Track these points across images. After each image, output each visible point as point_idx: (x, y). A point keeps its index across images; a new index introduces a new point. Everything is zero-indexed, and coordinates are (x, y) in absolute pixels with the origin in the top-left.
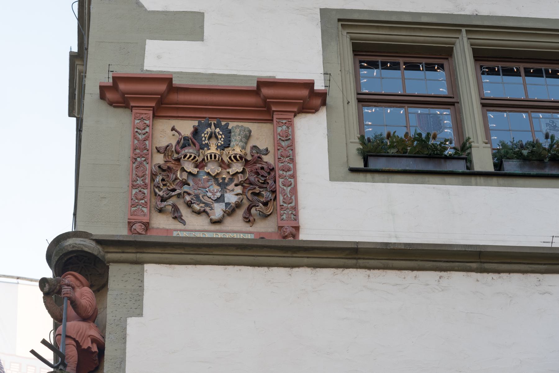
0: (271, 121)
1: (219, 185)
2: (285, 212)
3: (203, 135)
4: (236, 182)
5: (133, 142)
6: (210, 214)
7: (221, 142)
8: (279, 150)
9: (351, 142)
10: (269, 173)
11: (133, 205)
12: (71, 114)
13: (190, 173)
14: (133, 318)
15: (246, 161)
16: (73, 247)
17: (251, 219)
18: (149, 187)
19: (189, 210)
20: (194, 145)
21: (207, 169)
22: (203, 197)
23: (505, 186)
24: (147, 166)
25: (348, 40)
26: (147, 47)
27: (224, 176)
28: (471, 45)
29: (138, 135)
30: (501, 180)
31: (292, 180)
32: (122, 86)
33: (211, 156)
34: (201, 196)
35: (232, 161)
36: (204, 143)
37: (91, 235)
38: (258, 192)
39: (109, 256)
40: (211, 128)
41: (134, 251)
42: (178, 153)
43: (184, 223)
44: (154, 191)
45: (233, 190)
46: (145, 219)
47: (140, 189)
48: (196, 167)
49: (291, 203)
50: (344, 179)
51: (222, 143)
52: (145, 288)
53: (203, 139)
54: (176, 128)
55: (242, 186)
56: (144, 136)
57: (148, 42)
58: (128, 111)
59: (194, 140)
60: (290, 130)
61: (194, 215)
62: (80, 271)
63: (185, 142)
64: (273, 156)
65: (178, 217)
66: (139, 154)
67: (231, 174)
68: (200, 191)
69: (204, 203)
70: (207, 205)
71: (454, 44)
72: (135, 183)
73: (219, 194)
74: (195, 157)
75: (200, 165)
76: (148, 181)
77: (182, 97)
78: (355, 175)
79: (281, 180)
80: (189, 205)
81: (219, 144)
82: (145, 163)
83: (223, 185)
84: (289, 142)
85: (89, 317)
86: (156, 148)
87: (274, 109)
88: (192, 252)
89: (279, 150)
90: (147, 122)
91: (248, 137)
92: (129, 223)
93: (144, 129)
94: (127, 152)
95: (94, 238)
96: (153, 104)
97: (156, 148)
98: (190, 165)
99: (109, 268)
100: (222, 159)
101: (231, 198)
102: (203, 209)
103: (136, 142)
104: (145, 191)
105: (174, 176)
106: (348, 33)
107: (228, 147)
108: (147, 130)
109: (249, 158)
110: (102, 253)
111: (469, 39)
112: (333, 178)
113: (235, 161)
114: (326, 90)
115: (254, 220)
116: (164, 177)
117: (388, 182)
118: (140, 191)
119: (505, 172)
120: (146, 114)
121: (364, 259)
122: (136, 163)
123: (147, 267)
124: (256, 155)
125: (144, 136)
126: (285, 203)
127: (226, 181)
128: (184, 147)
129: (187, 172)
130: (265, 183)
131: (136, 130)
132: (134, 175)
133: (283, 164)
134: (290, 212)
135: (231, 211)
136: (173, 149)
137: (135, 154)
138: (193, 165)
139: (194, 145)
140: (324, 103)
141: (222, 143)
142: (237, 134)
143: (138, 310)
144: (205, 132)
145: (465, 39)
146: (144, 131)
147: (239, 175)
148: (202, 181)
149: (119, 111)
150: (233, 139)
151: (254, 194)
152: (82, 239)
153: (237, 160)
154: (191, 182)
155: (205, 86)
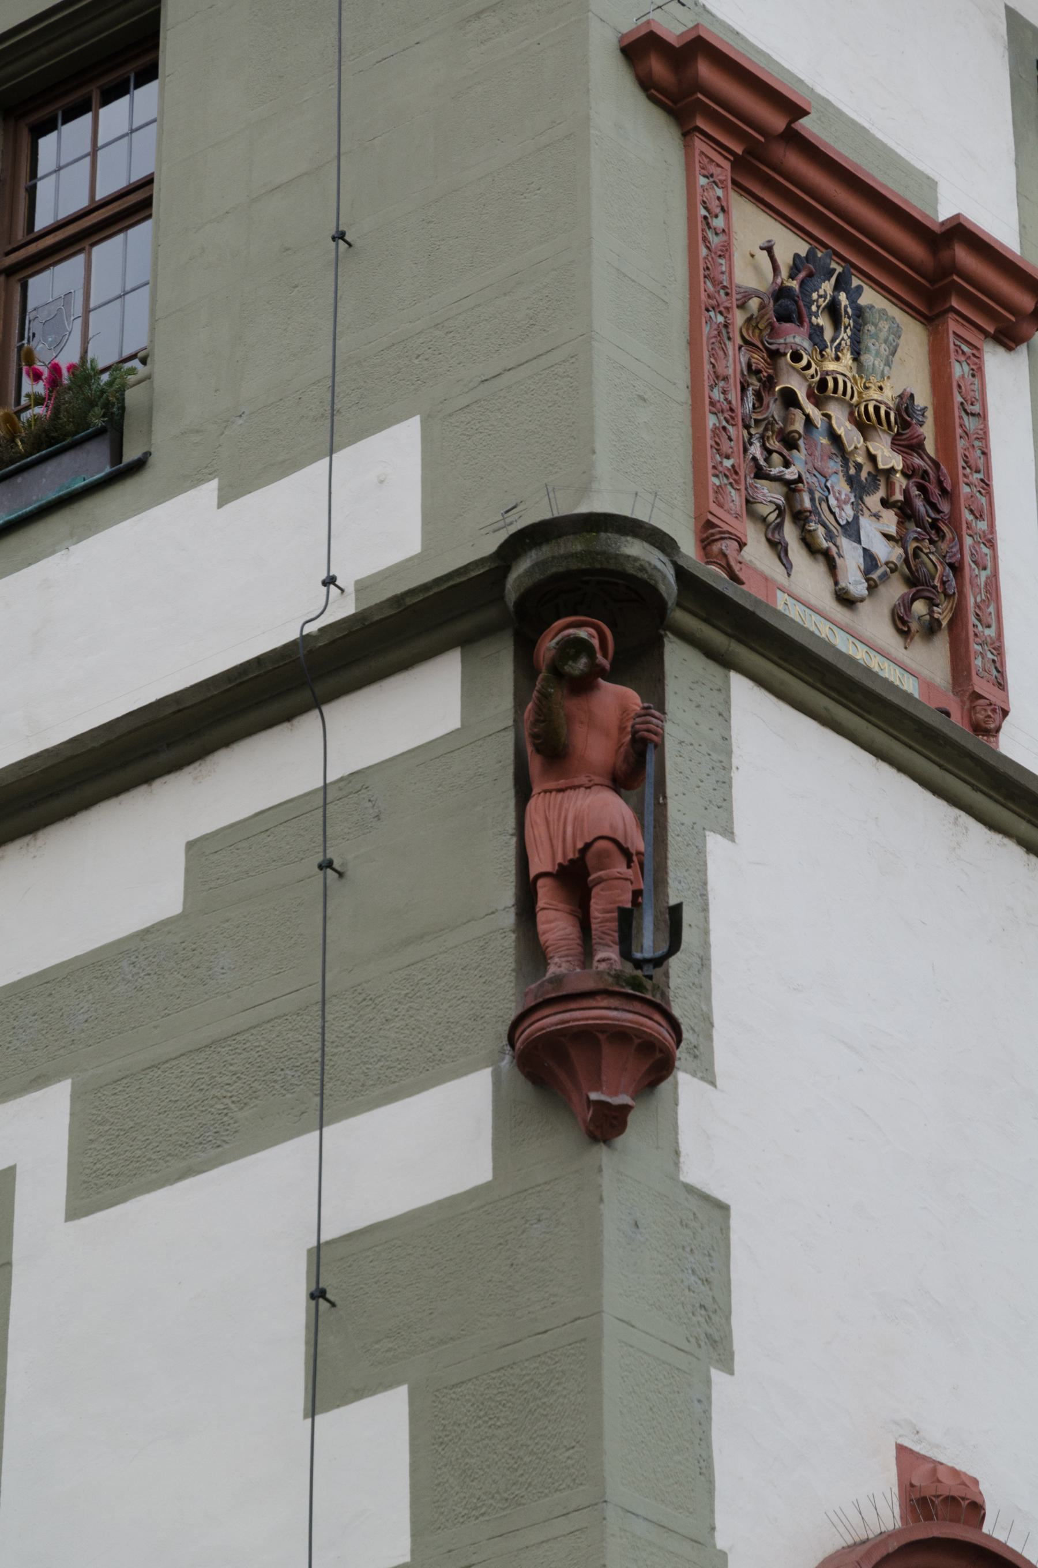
16: (642, 569)
41: (729, 631)
43: (788, 566)
77: (795, 162)
87: (955, 303)
88: (902, 737)
95: (680, 562)
96: (739, 150)
113: (885, 427)
120: (718, 165)
142: (883, 335)
155: (846, 158)
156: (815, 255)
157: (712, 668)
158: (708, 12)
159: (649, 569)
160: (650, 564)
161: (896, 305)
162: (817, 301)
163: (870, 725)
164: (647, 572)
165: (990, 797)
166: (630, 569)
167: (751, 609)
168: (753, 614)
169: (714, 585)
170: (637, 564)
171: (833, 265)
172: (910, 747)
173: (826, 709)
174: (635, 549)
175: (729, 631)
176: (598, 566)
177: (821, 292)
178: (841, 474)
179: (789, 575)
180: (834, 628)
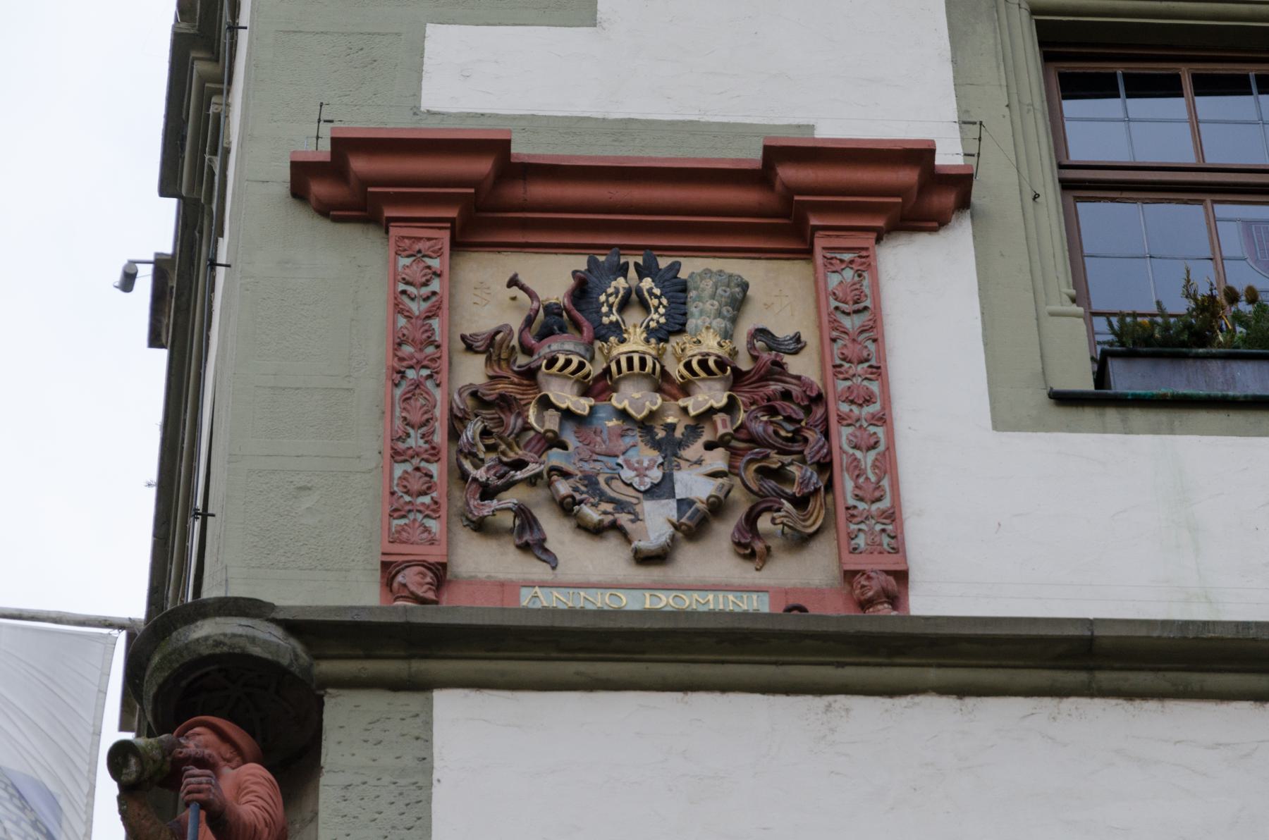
1: (657, 445)
3: (603, 298)
4: (707, 436)
5: (395, 322)
6: (633, 535)
7: (657, 318)
9: (1052, 314)
10: (808, 410)
11: (396, 512)
15: (737, 373)
16: (218, 643)
17: (759, 546)
19: (568, 524)
22: (607, 482)
24: (438, 394)
27: (670, 420)
31: (880, 431)
32: (360, 165)
33: (630, 360)
34: (601, 479)
36: (605, 320)
37: (272, 607)
38: (775, 466)
39: (326, 667)
40: (625, 277)
41: (402, 653)
42: (528, 351)
44: (460, 466)
45: (699, 462)
47: (416, 461)
48: (585, 392)
49: (879, 499)
51: (662, 320)
53: (605, 309)
54: (523, 279)
57: (431, 29)
60: (866, 282)
63: (551, 322)
65: (534, 547)
66: (411, 357)
67: (692, 413)
68: (598, 466)
69: (611, 500)
70: (620, 506)
72: (401, 446)
73: (656, 475)
74: (581, 366)
76: (440, 437)
79: (846, 431)
80: (567, 508)
81: (653, 324)
82: (429, 384)
83: (670, 448)
84: (865, 317)
86: (463, 338)
87: (814, 221)
90: (435, 263)
91: (738, 302)
92: (385, 566)
93: (425, 284)
94: (374, 353)
95: (281, 616)
96: (452, 213)
97: (463, 338)
99: (321, 704)
101: (695, 484)
102: (610, 518)
103: (402, 321)
104: (434, 468)
105: (520, 421)
108: (435, 285)
109: (745, 364)
113: (703, 375)
116: (489, 424)
117: (1172, 431)
118: (417, 469)
120: (429, 239)
121: (1113, 669)
124: (767, 357)
125: (424, 306)
126: (861, 499)
127: (678, 433)
128: (546, 333)
130: (795, 445)
133: (848, 383)
134: (878, 527)
135: (696, 525)
137: (401, 359)
138: (575, 389)
140: (964, 203)
141: (662, 320)
144: (610, 290)
146: (425, 291)
148: (605, 436)
150: (693, 309)
152: (244, 621)
154: (570, 438)
155: (543, 156)
156: (597, 261)
157: (403, 698)
158: (435, 114)
159: (227, 641)
160: (225, 635)
161: (759, 259)
162: (607, 301)
163: (649, 665)
164: (224, 644)
165: (867, 664)
166: (205, 651)
167: (402, 620)
168: (408, 623)
169: (338, 618)
170: (210, 642)
171: (622, 260)
172: (723, 662)
173: (577, 673)
174: (206, 629)
175: (402, 653)
176: (176, 665)
177: (610, 290)
178: (641, 445)
179: (554, 568)
180: (614, 591)
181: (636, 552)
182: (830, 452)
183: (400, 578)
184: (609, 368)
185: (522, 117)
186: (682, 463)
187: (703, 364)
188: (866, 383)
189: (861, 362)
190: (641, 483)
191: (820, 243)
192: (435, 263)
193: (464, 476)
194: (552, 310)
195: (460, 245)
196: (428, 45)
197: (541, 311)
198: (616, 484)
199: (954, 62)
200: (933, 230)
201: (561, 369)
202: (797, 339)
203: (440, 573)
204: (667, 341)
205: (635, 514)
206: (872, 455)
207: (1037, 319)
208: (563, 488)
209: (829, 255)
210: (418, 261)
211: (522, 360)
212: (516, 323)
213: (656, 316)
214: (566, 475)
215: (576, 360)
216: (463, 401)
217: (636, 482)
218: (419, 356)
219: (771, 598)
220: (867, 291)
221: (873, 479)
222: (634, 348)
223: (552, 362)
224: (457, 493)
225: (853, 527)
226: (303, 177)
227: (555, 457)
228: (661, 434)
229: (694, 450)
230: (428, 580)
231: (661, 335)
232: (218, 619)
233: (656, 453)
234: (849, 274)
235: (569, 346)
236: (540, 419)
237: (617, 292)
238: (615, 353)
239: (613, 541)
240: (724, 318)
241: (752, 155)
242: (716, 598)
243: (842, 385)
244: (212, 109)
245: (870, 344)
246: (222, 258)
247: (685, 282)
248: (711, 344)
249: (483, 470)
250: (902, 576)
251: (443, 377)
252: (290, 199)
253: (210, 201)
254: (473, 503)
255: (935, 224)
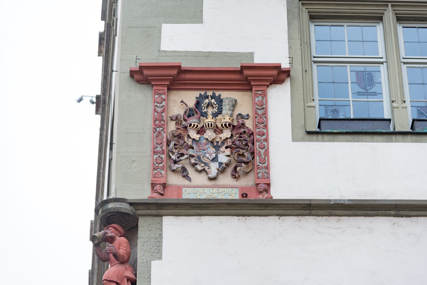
0: (251, 90)
1: (214, 147)
2: (260, 171)
3: (203, 105)
4: (226, 145)
5: (154, 114)
6: (208, 173)
7: (215, 110)
8: (256, 117)
9: (308, 107)
10: (250, 136)
11: (155, 169)
12: (102, 19)
13: (194, 139)
14: (156, 261)
15: (234, 126)
17: (237, 175)
18: (165, 153)
19: (193, 169)
20: (197, 113)
21: (206, 136)
22: (203, 157)
23: (417, 142)
24: (164, 135)
25: (307, 13)
26: (163, 31)
27: (218, 140)
28: (396, 14)
29: (157, 108)
30: (414, 138)
31: (265, 143)
32: (146, 72)
33: (208, 124)
34: (201, 157)
35: (223, 128)
36: (203, 111)
37: (126, 200)
38: (241, 153)
39: (139, 212)
40: (208, 99)
42: (185, 120)
44: (169, 155)
45: (224, 152)
46: (162, 181)
47: (159, 154)
48: (198, 133)
49: (264, 163)
50: (303, 140)
51: (217, 111)
52: (163, 236)
53: (203, 108)
54: (184, 101)
55: (230, 148)
56: (161, 109)
57: (163, 24)
58: (149, 87)
59: (196, 110)
60: (264, 100)
61: (197, 173)
62: (119, 227)
63: (190, 113)
64: (252, 120)
65: (186, 177)
66: (158, 125)
67: (223, 139)
68: (201, 153)
69: (204, 163)
70: (206, 164)
71: (383, 14)
72: (156, 150)
73: (214, 155)
74: (197, 126)
75: (201, 131)
76: (164, 148)
78: (310, 137)
79: (258, 143)
80: (194, 165)
81: (214, 112)
82: (162, 132)
83: (217, 148)
84: (264, 110)
85: (128, 260)
86: (170, 117)
87: (252, 84)
89: (256, 117)
90: (163, 96)
91: (234, 104)
92: (152, 184)
93: (161, 103)
94: (149, 123)
95: (128, 202)
96: (168, 83)
97: (170, 117)
98: (194, 132)
99: (138, 220)
100: (216, 125)
101: (223, 158)
102: (203, 168)
103: (156, 114)
104: (163, 156)
105: (183, 142)
106: (306, 8)
107: (221, 113)
108: (164, 103)
109: (235, 124)
110: (134, 211)
111: (394, 10)
112: (294, 139)
113: (225, 128)
114: (289, 68)
115: (239, 176)
116: (176, 142)
117: (333, 141)
118: (159, 157)
119: (416, 131)
121: (315, 210)
122: (156, 132)
123: (164, 218)
124: (241, 121)
125: (161, 109)
126: (261, 163)
127: (219, 144)
128: (189, 116)
129: (192, 139)
130: (247, 147)
131: (156, 104)
132: (155, 143)
133: (259, 130)
134: (264, 171)
135: (222, 170)
136: (182, 119)
137: (156, 125)
138: (196, 132)
139: (197, 113)
140: (289, 76)
141: (217, 111)
143: (158, 254)
144: (205, 103)
145: (391, 13)
146: (161, 105)
147: (228, 140)
148: (202, 145)
149: (143, 87)
150: (224, 108)
151: (239, 155)
152: (120, 203)
153: (227, 127)
154: (195, 146)
174: (111, 206)
177: (205, 103)
181: (209, 178)
182: (254, 150)
183: (155, 188)
184: (203, 126)
185: (185, 52)
186: (220, 152)
187: (225, 125)
188: (263, 130)
189: (262, 124)
190: (211, 158)
191: (254, 89)
192: (163, 96)
193: (170, 157)
194: (191, 110)
195: (170, 89)
196: (162, 30)
197: (188, 110)
198: (205, 158)
199: (288, 33)
200: (281, 84)
201: (193, 127)
202: (248, 115)
203: (164, 186)
204: (217, 116)
205: (209, 166)
206: (264, 150)
207: (304, 109)
208: (193, 161)
209: (256, 92)
210: (160, 96)
211: (184, 123)
212: (182, 113)
213: (215, 110)
214: (193, 156)
215: (196, 124)
216: (170, 137)
217: (209, 157)
218: (160, 124)
219: (239, 190)
220: (264, 103)
221: (263, 157)
222: (210, 120)
223: (190, 125)
224: (168, 161)
225: (259, 171)
226: (132, 73)
227: (191, 152)
228: (215, 144)
229: (223, 149)
230: (162, 188)
231: (215, 115)
232: (114, 203)
233: (214, 149)
234: (260, 97)
235: (194, 120)
236: (187, 140)
237: (206, 103)
238: (205, 121)
239: (204, 174)
240: (231, 110)
241: (237, 66)
242: (227, 190)
243: (258, 130)
244: (113, 7)
245: (264, 118)
246: (114, 69)
247: (222, 100)
248: (227, 119)
249: (174, 155)
250: (269, 185)
251: (165, 130)
252: (130, 78)
253: (113, 26)
254: (172, 165)
255: (281, 82)
